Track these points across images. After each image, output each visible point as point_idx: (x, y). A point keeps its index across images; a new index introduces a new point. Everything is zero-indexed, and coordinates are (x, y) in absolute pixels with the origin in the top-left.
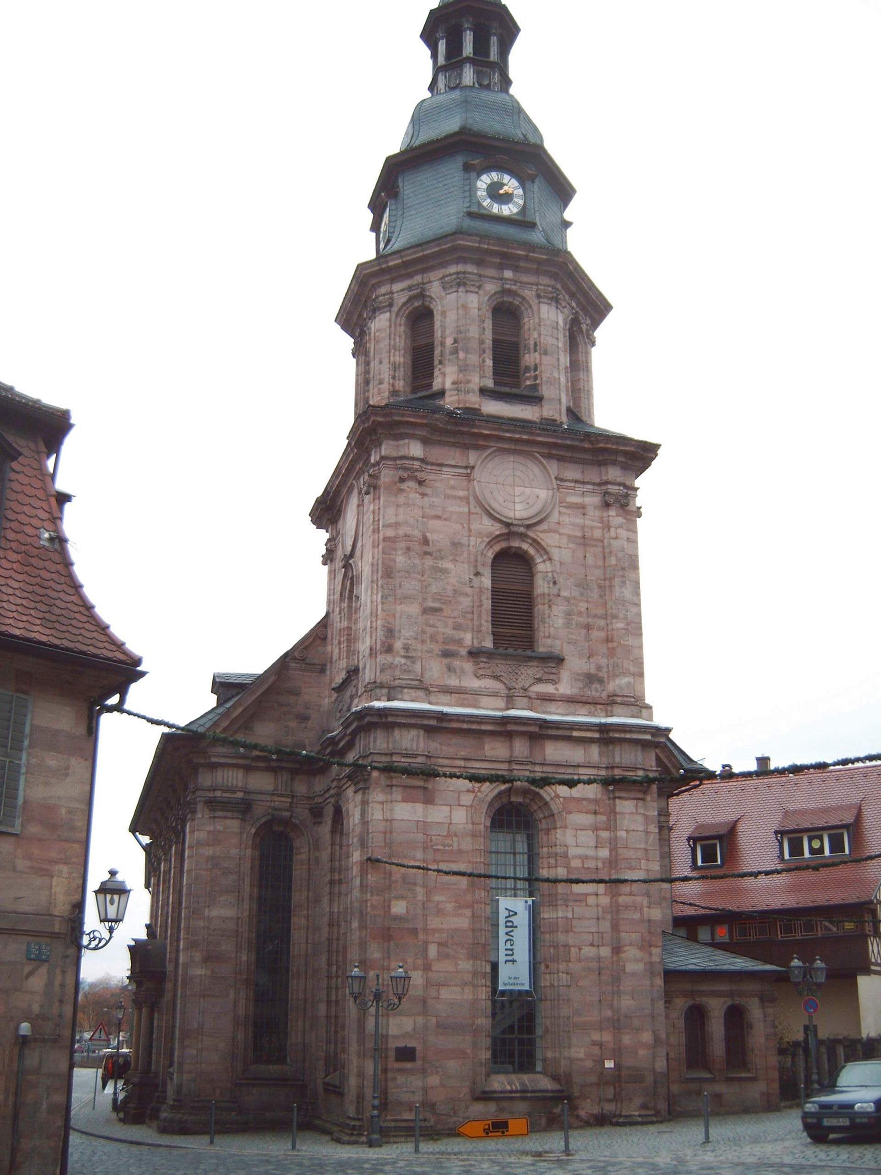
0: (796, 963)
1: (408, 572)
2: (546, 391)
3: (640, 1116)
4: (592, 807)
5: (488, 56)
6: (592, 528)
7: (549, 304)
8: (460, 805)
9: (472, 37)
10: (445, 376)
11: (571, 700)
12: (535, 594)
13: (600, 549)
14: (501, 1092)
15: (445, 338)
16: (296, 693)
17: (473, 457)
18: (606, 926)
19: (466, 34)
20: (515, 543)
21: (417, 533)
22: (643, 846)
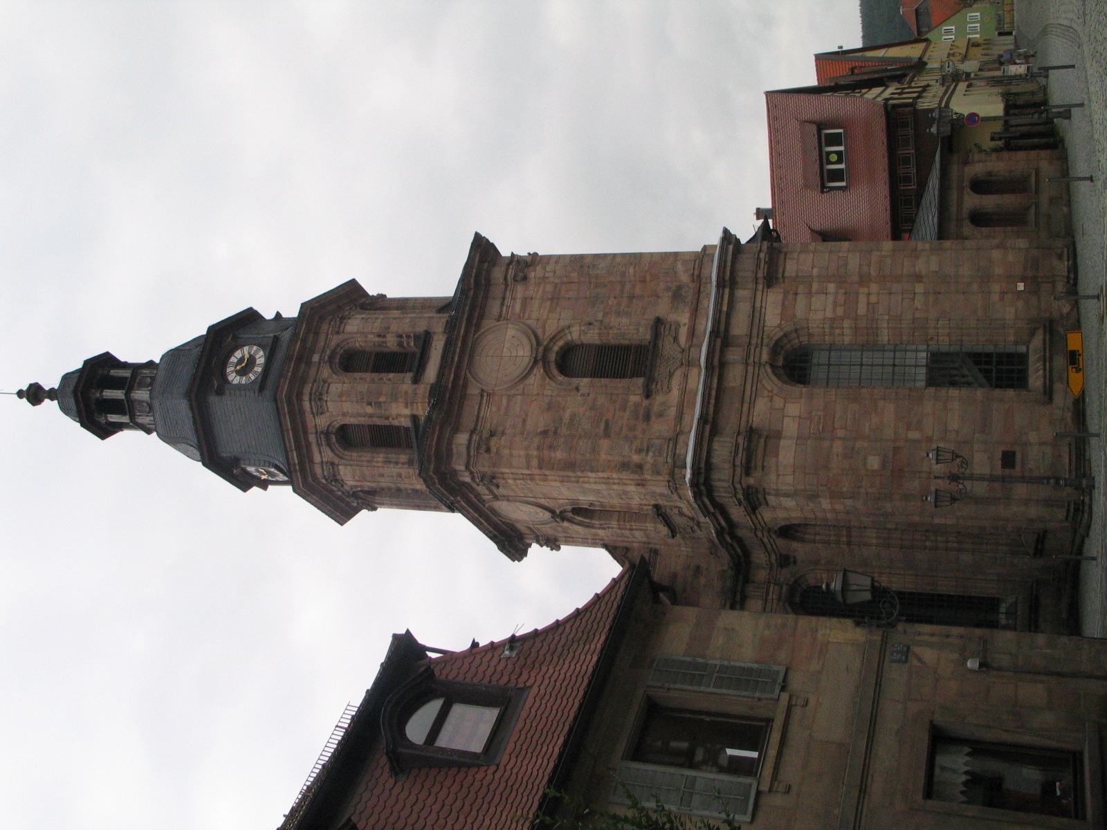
0: (934, 130)
1: (571, 448)
2: (421, 328)
3: (1068, 261)
4: (790, 296)
5: (126, 378)
7: (345, 324)
8: (783, 409)
9: (108, 391)
10: (400, 415)
11: (695, 313)
12: (598, 342)
14: (1045, 378)
15: (367, 414)
16: (674, 576)
17: (473, 390)
18: (896, 287)
19: (106, 396)
20: (552, 357)
21: (536, 440)
22: (827, 255)
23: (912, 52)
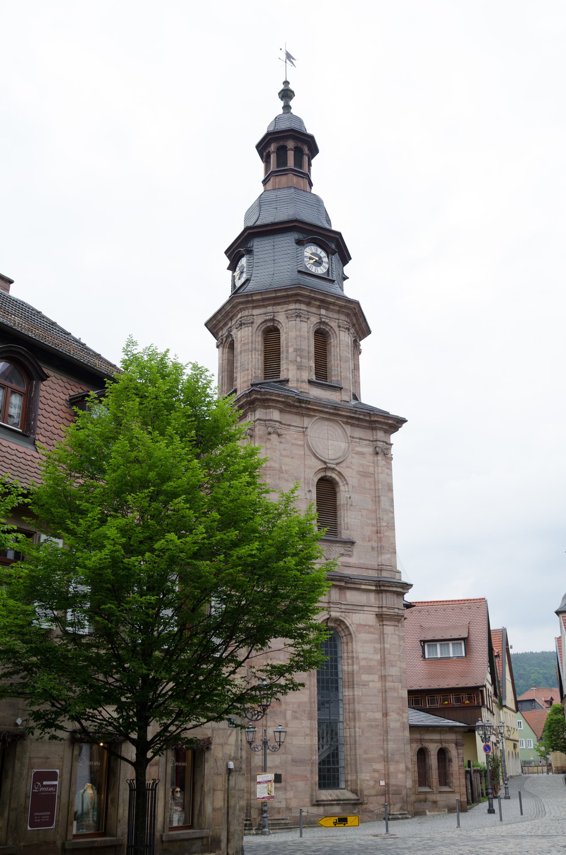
6: (369, 466)
13: (373, 479)
14: (327, 801)
17: (307, 421)
20: (329, 474)
23: (509, 701)
